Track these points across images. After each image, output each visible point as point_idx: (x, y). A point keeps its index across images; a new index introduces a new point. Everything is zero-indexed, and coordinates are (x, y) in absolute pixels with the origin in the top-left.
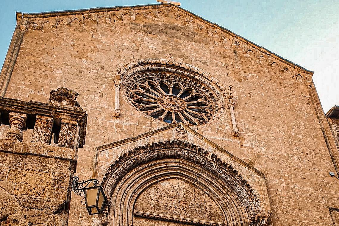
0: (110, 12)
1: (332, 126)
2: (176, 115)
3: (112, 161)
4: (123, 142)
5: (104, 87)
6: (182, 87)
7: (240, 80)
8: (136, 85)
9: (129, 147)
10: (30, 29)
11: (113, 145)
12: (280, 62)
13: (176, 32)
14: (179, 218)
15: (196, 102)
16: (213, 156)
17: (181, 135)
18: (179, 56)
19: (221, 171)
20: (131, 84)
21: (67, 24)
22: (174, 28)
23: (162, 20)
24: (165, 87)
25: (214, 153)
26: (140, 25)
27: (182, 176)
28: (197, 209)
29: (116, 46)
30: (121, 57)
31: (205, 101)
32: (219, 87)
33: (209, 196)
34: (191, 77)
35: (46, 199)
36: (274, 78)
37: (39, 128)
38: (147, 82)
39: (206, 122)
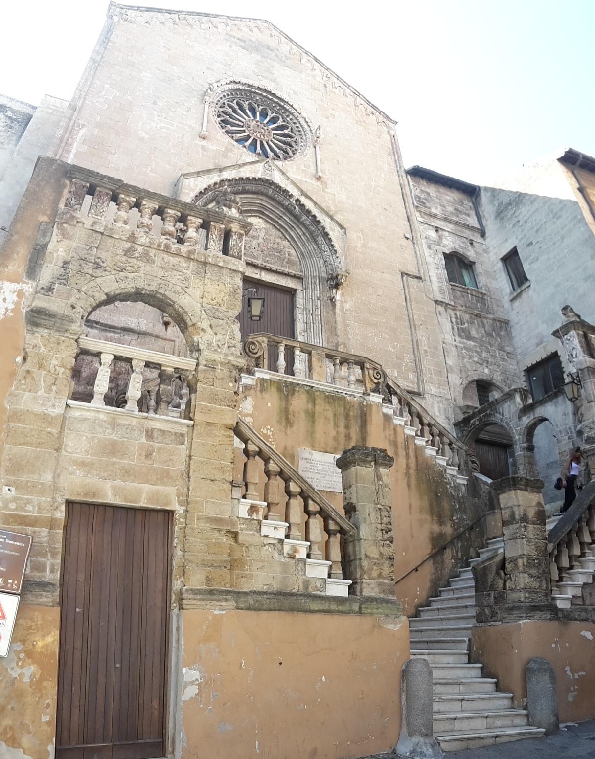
0: (206, 18)
1: (411, 184)
2: (262, 143)
3: (196, 192)
4: (209, 171)
5: (193, 102)
6: (270, 112)
7: (327, 118)
8: (224, 103)
9: (215, 178)
10: (121, 21)
11: (198, 174)
12: (367, 105)
13: (270, 52)
14: (257, 261)
15: (282, 132)
16: (298, 200)
17: (268, 172)
18: (271, 80)
19: (304, 217)
20: (219, 101)
21: (161, 23)
22: (268, 48)
23: (256, 36)
24: (253, 110)
25: (299, 197)
26: (234, 37)
27: (263, 215)
28: (276, 254)
29: (209, 56)
30: (214, 71)
31: (291, 133)
32: (307, 122)
33: (288, 241)
34: (280, 105)
35: (225, 310)
36: (360, 121)
37: (214, 235)
38: (235, 102)
39: (290, 157)
